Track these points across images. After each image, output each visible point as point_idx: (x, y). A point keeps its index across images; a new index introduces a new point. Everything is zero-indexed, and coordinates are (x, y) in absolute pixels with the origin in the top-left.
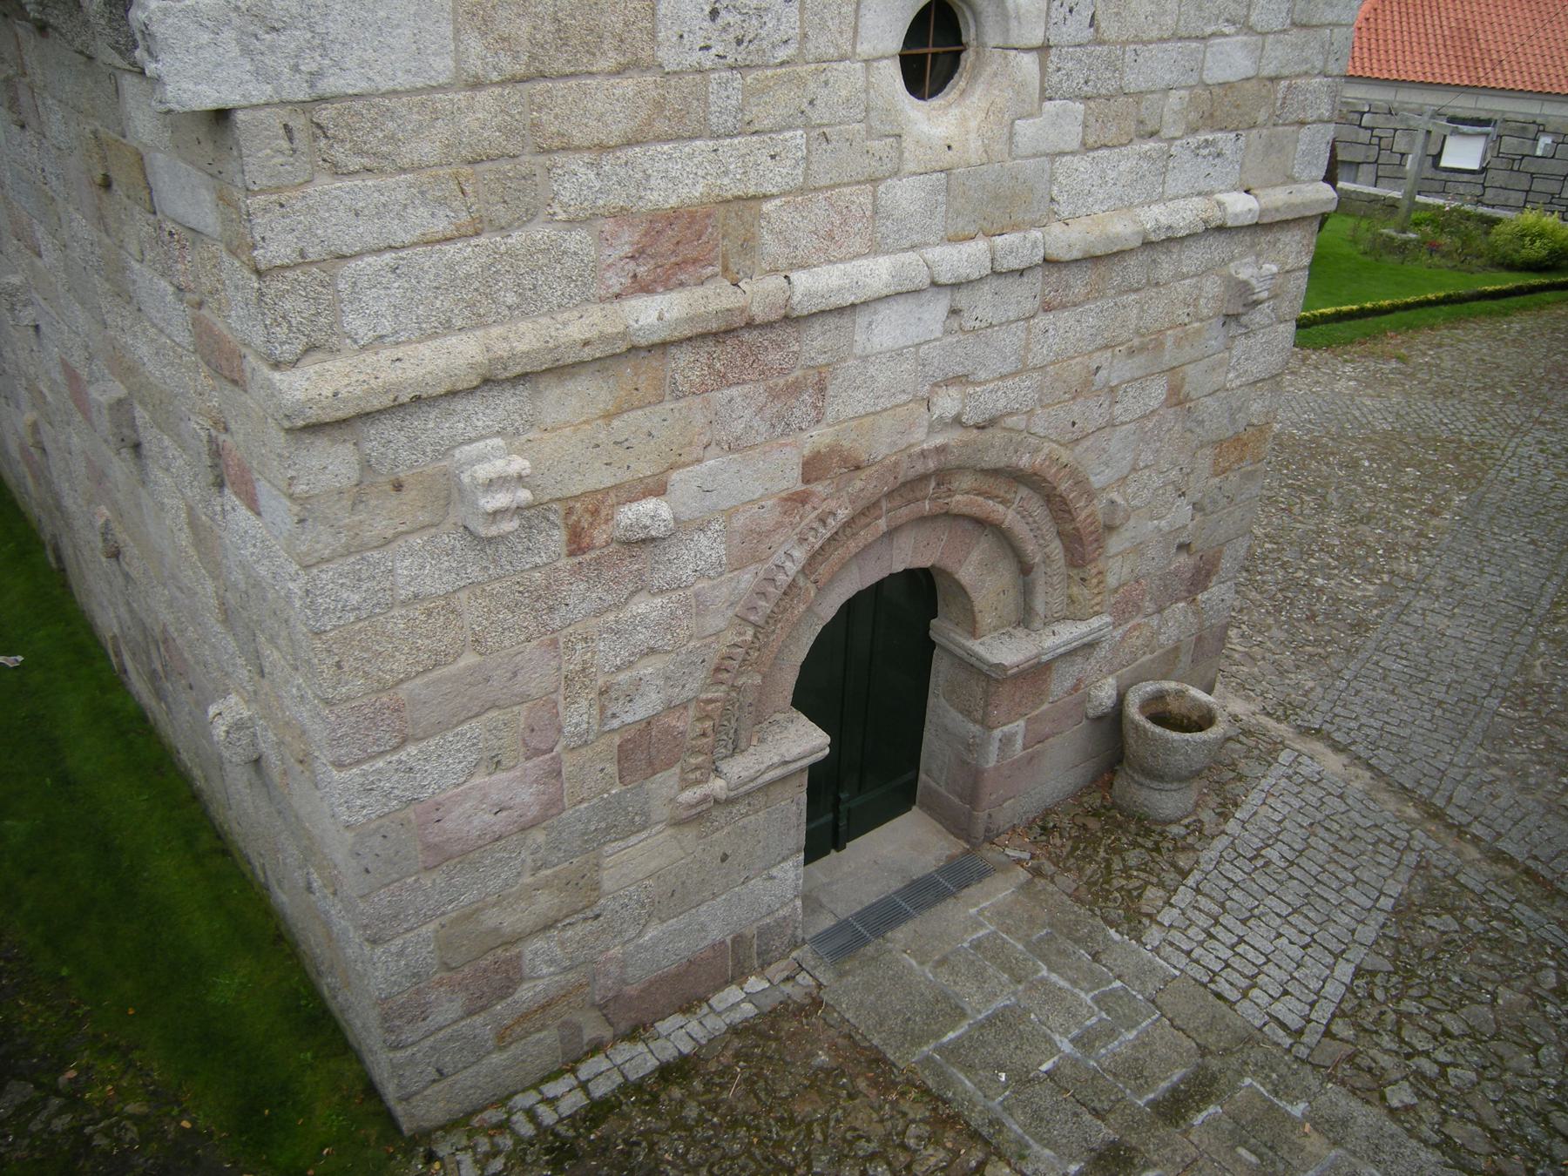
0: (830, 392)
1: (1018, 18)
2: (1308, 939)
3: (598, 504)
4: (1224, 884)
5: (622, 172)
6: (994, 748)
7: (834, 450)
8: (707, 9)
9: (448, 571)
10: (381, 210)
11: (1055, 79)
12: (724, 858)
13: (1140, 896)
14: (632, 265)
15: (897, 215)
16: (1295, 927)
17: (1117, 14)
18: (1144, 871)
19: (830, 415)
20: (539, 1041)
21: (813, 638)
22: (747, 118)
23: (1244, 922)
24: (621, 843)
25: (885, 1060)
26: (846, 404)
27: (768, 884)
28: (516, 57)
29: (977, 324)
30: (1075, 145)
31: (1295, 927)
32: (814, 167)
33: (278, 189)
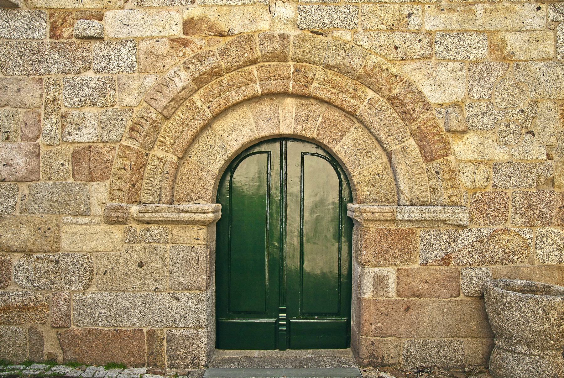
3: (66, 15)
20: (16, 332)
25: (184, 67)
30: (408, 203)
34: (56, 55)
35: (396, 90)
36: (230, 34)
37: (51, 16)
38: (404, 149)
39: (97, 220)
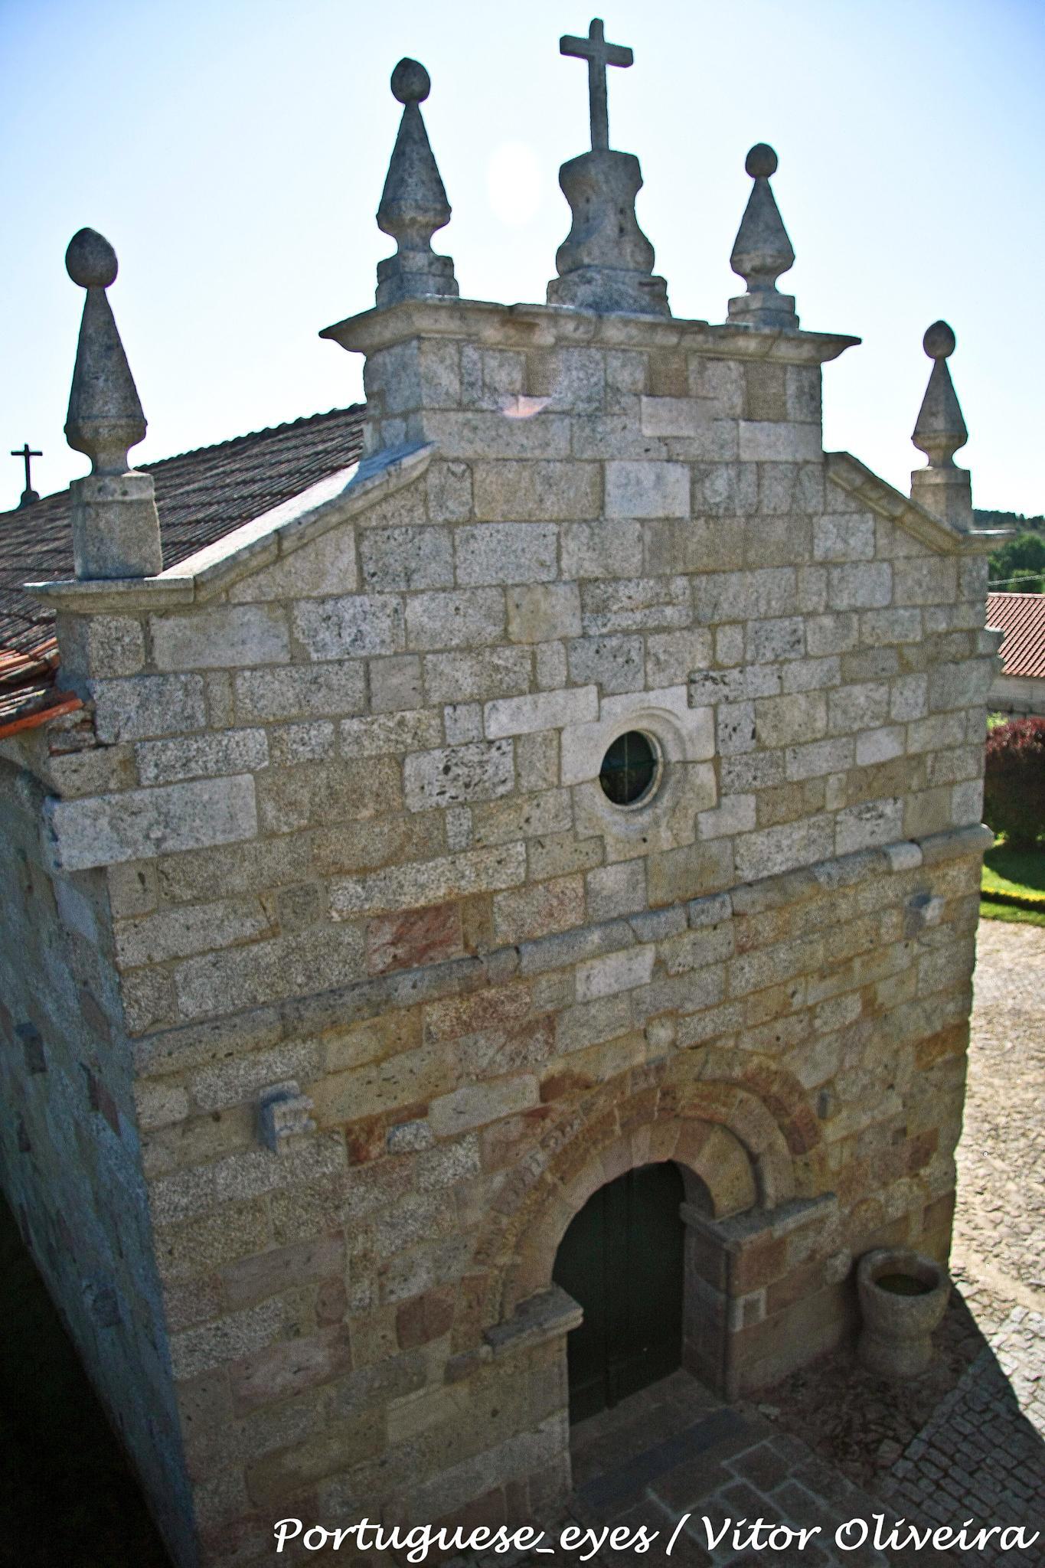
0: (559, 1030)
1: (691, 740)
2: (1031, 1492)
4: (955, 1437)
5: (382, 884)
6: (739, 1313)
7: (566, 1075)
8: (441, 766)
9: (255, 1180)
10: (205, 925)
11: (728, 780)
12: (495, 1413)
13: (876, 1450)
14: (392, 950)
15: (605, 893)
16: (1019, 1480)
17: (775, 726)
18: (882, 1425)
19: (560, 1046)
21: (567, 1224)
22: (477, 837)
23: (971, 1474)
24: (403, 1400)
26: (575, 1036)
27: (536, 1436)
28: (301, 815)
29: (681, 969)
31: (1019, 1480)
32: (533, 866)
33: (134, 917)
34: (362, 1189)
35: (775, 1088)
36: (600, 1082)
37: (349, 1132)
38: (771, 1146)
39: (436, 1386)
